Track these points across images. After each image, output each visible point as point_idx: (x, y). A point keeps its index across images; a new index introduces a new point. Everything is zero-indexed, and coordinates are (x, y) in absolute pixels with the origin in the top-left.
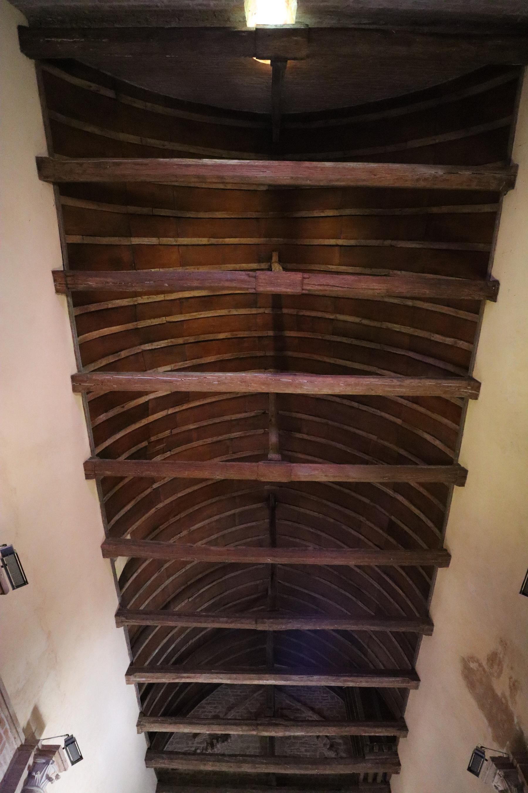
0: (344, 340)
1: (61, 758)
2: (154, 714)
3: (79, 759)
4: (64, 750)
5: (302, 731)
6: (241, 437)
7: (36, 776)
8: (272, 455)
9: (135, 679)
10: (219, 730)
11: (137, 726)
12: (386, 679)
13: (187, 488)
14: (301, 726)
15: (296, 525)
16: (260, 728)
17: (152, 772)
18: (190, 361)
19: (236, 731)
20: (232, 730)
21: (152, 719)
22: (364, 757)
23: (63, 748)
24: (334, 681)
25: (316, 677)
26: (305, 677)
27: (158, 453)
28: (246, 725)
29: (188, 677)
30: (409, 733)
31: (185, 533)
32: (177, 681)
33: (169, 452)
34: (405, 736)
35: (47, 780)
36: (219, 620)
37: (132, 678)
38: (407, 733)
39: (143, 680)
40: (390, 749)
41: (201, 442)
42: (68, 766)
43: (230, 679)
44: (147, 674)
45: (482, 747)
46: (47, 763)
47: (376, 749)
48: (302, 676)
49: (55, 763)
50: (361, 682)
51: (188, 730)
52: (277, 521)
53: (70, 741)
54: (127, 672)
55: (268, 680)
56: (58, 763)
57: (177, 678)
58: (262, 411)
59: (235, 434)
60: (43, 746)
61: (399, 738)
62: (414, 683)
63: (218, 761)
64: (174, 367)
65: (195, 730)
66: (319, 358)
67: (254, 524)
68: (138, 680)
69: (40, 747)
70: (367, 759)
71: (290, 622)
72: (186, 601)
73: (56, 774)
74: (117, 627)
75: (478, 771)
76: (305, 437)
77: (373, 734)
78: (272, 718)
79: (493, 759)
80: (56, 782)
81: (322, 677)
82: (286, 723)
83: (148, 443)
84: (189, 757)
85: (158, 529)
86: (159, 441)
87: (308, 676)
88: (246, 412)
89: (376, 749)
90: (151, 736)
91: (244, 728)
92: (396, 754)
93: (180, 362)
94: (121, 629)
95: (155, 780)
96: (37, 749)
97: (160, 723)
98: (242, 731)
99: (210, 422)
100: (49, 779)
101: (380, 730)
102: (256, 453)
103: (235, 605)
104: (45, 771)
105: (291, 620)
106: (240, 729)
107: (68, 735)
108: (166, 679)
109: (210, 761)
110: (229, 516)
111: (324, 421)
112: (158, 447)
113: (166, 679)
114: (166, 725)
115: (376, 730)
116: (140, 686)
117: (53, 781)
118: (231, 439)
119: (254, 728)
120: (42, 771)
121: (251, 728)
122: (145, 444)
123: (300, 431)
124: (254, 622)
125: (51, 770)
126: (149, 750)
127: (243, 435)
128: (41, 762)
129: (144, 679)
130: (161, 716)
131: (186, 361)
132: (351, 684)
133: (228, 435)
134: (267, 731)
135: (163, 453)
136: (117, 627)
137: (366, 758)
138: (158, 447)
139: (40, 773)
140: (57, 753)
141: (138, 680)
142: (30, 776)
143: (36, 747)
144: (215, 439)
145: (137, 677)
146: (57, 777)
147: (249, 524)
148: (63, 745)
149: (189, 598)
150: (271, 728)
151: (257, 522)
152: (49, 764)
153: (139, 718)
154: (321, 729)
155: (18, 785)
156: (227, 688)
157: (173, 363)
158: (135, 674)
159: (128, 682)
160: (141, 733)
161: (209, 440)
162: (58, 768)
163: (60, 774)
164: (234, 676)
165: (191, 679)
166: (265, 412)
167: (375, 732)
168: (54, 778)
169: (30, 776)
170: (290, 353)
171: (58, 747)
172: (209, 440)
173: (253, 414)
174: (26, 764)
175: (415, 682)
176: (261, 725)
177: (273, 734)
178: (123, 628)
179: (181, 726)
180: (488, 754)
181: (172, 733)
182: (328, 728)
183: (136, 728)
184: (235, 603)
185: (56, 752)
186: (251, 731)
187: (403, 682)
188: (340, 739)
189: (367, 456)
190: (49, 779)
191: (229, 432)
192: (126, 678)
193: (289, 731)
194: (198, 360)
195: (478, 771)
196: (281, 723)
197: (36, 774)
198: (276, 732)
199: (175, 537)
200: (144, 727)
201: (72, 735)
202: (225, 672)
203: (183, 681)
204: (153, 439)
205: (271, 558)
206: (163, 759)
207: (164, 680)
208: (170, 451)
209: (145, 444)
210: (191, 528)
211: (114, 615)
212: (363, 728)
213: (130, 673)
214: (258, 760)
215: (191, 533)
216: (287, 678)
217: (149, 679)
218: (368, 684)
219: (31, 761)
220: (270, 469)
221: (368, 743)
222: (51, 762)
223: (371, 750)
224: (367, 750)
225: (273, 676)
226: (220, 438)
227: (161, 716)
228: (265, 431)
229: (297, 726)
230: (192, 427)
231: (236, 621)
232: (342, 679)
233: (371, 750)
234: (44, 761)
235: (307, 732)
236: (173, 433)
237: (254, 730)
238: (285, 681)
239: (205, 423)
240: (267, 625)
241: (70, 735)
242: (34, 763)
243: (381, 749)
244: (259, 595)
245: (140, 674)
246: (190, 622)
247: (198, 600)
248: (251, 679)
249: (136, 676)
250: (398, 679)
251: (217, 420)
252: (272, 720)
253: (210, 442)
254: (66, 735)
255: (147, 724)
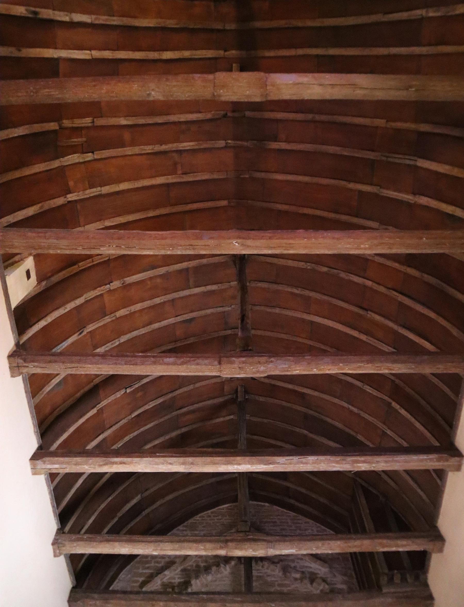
2: (75, 530)
5: (291, 549)
6: (193, 151)
8: (236, 437)
9: (44, 466)
10: (171, 550)
11: (53, 544)
12: (415, 457)
13: (119, 216)
14: (290, 541)
15: (275, 287)
16: (230, 544)
18: (118, 18)
19: (197, 549)
20: (190, 548)
21: (74, 537)
22: (380, 588)
24: (337, 462)
25: (311, 458)
26: (295, 459)
27: (74, 150)
28: (210, 541)
29: (121, 463)
30: (447, 544)
31: (116, 284)
33: (90, 154)
34: (441, 550)
36: (163, 360)
37: (40, 464)
38: (443, 544)
40: (417, 578)
41: (136, 150)
43: (183, 464)
44: (61, 459)
47: (397, 579)
48: (291, 457)
50: (378, 462)
51: (127, 549)
52: (248, 284)
54: (31, 457)
55: (240, 464)
57: (106, 464)
58: (222, 113)
59: (185, 144)
61: (430, 554)
62: (454, 461)
63: (172, 601)
64: (96, 19)
65: (136, 550)
66: (300, 24)
67: (214, 287)
68: (49, 466)
70: (385, 593)
71: (272, 362)
72: (123, 392)
74: (12, 376)
76: (283, 146)
78: (247, 533)
81: (322, 458)
82: (269, 538)
83: (60, 128)
84: (132, 596)
85: (76, 266)
86: (77, 130)
87: (299, 457)
88: (200, 112)
89: (397, 579)
91: (208, 545)
92: (426, 585)
93: (104, 15)
94: (19, 379)
97: (86, 541)
98: (205, 550)
99: (150, 121)
101: (404, 542)
102: (215, 176)
103: (193, 411)
105: (272, 359)
106: (202, 548)
109: (161, 601)
110: (180, 272)
111: (310, 116)
112: (76, 140)
114: (95, 544)
115: (399, 542)
116: (52, 476)
118: (180, 152)
119: (222, 545)
121: (218, 545)
122: (53, 126)
123: (275, 139)
124: (216, 363)
126: (74, 590)
127: (197, 147)
129: (57, 466)
130: (85, 533)
131: (114, 16)
133: (176, 144)
134: (241, 549)
135: (83, 153)
136: (12, 376)
137: (385, 590)
138: (76, 140)
141: (49, 466)
144: (158, 148)
145: (47, 463)
147: (209, 288)
149: (126, 388)
150: (247, 545)
151: (220, 285)
153: (56, 535)
154: (320, 544)
156: (186, 530)
157: (94, 14)
158: (44, 459)
159: (35, 472)
160: (58, 556)
161: (148, 149)
164: (190, 459)
165: (127, 466)
166: (226, 114)
167: (397, 546)
170: (258, 24)
172: (148, 149)
173: (209, 116)
175: (457, 459)
176: (232, 541)
178: (21, 377)
179: (117, 544)
182: (330, 542)
183: (50, 548)
184: (191, 408)
186: (217, 549)
187: (439, 460)
188: (342, 583)
189: (373, 153)
191: (178, 140)
192: (31, 464)
193: (274, 548)
194: (129, 19)
196: (261, 538)
198: (254, 550)
199: (102, 288)
200: (64, 546)
202: (177, 455)
204: (67, 123)
205: (239, 241)
206: (93, 598)
208: (93, 152)
209: (53, 126)
210: (125, 279)
211: (6, 354)
212: (380, 541)
213: (35, 457)
214: (230, 597)
215: (126, 287)
216: (269, 461)
217: (64, 466)
218: (388, 465)
220: (234, 77)
221: (386, 571)
223: (391, 580)
224: (384, 580)
225: (247, 458)
226: (164, 147)
227: (85, 533)
228: (226, 143)
229: (285, 541)
230: (123, 122)
231: (189, 361)
232: (350, 459)
233: (391, 580)
235: (300, 549)
236: (95, 125)
237: (221, 548)
238: (265, 464)
239: (141, 121)
240: (236, 365)
243: (404, 579)
244: (226, 398)
245: (52, 458)
246: (119, 364)
247: (139, 394)
248: (215, 464)
249: (45, 462)
250: (431, 456)
251: (159, 120)
252: (248, 535)
253: (150, 151)
255: (67, 543)
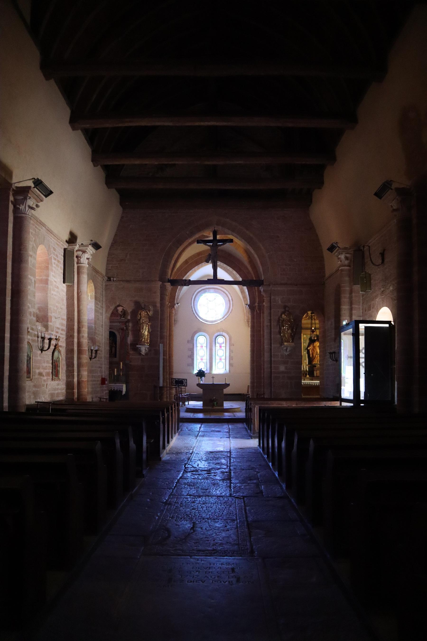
0: (168, 332)
1: (35, 194)
3: (50, 193)
4: (35, 189)
7: (20, 207)
17: (114, 191)
23: (34, 188)
32: (120, 125)
35: (30, 209)
39: (88, 126)
42: (43, 198)
45: (391, 181)
46: (25, 199)
49: (32, 198)
53: (38, 183)
56: (34, 198)
60: (16, 187)
69: (15, 189)
73: (35, 204)
75: (382, 196)
77: (304, 163)
79: (397, 189)
80: (38, 209)
90: (106, 168)
95: (118, 196)
96: (12, 190)
100: (32, 208)
104: (26, 203)
107: (35, 179)
108: (109, 124)
113: (109, 124)
117: (35, 209)
120: (24, 204)
125: (31, 202)
128: (20, 198)
129: (88, 126)
132: (290, 125)
139: (23, 205)
140: (30, 191)
142: (16, 210)
143: (11, 189)
146: (37, 206)
148: (33, 186)
152: (27, 199)
155: (9, 215)
162: (35, 201)
163: (38, 204)
168: (35, 207)
169: (16, 210)
171: (29, 187)
174: (9, 201)
177: (215, 163)
180: (394, 186)
181: (123, 165)
185: (29, 191)
190: (32, 208)
195: (382, 196)
197: (19, 206)
201: (38, 178)
203: (126, 125)
207: (107, 125)
219: (11, 198)
222: (28, 198)
234: (22, 197)
241: (36, 178)
242: (15, 199)
254: (33, 179)
